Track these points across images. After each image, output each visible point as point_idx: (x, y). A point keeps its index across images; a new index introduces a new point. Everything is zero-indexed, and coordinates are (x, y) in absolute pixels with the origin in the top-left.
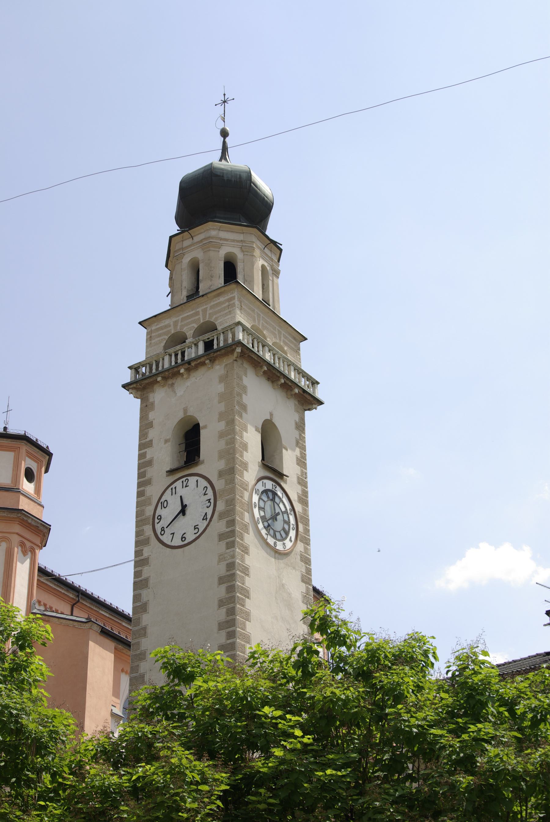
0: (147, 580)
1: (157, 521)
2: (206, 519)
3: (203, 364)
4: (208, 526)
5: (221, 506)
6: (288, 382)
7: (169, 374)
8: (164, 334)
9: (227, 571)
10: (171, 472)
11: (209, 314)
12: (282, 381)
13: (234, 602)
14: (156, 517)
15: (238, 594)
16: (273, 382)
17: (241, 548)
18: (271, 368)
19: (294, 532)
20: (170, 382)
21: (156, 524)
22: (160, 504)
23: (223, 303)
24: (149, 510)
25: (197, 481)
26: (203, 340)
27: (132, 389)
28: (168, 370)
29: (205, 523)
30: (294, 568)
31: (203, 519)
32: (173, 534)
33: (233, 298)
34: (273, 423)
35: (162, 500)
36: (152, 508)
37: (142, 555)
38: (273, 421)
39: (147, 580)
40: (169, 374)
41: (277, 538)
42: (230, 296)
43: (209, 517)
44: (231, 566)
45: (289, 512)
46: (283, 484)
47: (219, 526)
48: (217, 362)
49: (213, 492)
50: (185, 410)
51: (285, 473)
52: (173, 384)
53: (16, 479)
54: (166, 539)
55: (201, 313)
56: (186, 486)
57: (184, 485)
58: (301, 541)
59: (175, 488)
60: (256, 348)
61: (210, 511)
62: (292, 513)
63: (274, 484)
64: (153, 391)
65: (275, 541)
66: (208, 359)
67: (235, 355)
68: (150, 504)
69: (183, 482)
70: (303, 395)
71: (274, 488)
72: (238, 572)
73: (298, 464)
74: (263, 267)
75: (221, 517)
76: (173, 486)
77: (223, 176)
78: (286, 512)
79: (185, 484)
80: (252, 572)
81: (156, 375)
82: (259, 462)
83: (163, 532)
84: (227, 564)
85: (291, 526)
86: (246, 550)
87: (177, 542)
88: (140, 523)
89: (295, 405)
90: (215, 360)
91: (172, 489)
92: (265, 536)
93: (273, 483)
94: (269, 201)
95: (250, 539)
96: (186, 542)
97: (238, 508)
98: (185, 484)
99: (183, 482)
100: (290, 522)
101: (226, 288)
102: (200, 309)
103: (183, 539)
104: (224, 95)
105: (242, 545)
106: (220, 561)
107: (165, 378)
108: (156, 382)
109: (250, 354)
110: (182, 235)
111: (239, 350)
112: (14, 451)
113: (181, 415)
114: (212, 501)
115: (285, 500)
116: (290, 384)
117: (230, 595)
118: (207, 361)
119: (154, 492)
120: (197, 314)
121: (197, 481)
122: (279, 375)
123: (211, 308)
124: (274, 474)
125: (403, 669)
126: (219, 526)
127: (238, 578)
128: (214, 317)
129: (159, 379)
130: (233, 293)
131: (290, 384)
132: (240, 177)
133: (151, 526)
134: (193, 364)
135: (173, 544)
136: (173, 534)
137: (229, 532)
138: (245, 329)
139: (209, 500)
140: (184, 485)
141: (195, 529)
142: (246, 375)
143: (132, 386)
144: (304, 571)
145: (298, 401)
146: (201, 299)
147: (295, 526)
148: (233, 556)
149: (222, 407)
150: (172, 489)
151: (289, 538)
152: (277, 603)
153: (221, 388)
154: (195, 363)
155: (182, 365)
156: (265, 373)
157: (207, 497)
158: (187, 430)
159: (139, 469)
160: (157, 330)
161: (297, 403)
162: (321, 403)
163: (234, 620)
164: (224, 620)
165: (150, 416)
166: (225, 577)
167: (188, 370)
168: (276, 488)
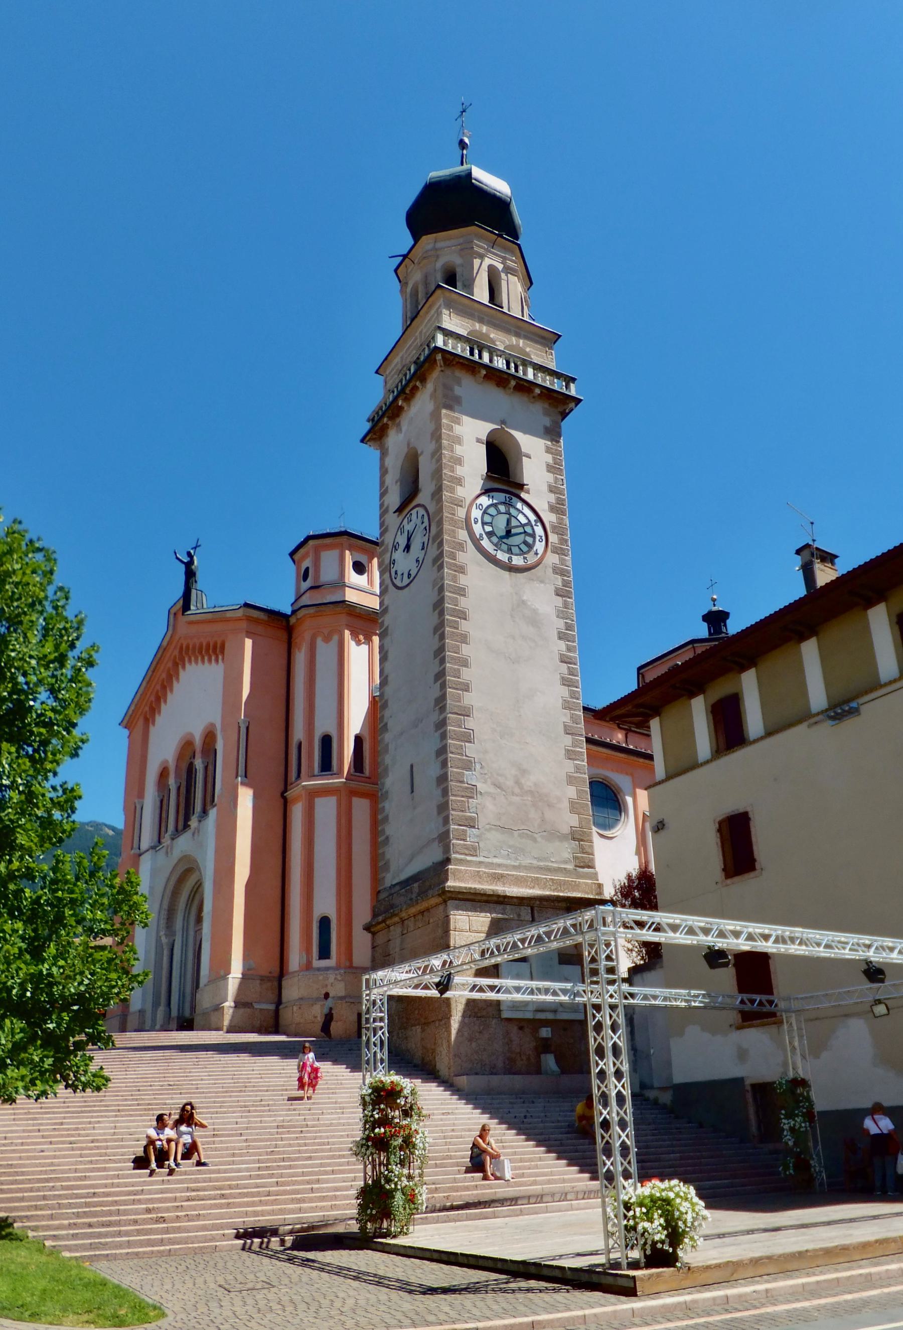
15: (447, 617)
16: (504, 387)
17: (453, 568)
18: (448, 356)
27: (368, 441)
28: (386, 410)
30: (542, 582)
45: (533, 523)
47: (433, 551)
58: (553, 552)
60: (521, 372)
61: (426, 539)
63: (508, 496)
65: (509, 555)
71: (508, 499)
73: (548, 471)
78: (529, 523)
82: (482, 475)
87: (406, 581)
92: (494, 553)
93: (844, 566)
94: (503, 196)
95: (469, 556)
100: (535, 534)
102: (417, 334)
114: (428, 528)
115: (526, 510)
118: (418, 384)
120: (416, 339)
122: (506, 376)
124: (500, 483)
129: (385, 420)
134: (407, 391)
142: (459, 384)
143: (368, 438)
147: (544, 538)
152: (514, 621)
156: (486, 377)
161: (546, 406)
162: (578, 401)
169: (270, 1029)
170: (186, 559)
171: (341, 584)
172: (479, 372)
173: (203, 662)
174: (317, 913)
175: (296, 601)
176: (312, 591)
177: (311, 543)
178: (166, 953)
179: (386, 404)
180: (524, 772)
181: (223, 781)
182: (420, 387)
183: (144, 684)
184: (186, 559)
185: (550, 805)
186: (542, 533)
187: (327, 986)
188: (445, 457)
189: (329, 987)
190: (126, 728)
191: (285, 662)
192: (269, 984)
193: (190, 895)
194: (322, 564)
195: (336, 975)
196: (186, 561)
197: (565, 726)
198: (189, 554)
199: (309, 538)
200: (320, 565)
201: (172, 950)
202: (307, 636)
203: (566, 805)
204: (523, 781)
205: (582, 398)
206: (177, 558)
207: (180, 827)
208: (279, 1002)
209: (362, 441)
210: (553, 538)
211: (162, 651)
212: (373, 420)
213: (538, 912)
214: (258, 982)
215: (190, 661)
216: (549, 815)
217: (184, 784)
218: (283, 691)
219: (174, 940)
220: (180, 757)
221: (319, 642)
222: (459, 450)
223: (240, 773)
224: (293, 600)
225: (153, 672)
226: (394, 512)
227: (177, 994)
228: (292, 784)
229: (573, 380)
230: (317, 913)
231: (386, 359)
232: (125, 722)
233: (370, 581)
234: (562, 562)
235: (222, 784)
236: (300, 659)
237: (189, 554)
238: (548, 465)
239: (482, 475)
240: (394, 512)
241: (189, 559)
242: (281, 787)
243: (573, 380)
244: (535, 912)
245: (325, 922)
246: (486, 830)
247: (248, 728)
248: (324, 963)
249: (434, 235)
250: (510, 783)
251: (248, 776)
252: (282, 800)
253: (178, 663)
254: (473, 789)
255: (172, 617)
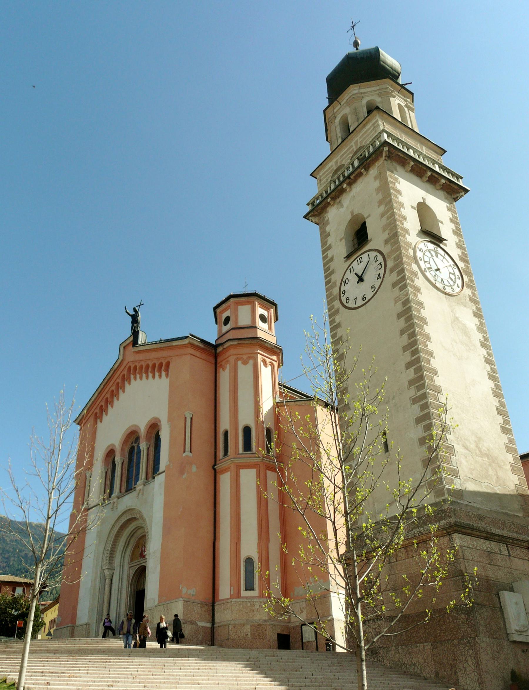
0: (341, 338)
1: (342, 295)
2: (380, 278)
3: (360, 174)
4: (382, 282)
5: (390, 264)
6: (434, 174)
7: (336, 193)
8: (330, 173)
9: (403, 307)
10: (348, 257)
11: (360, 142)
12: (429, 173)
13: (413, 327)
14: (341, 292)
15: (416, 321)
18: (393, 150)
19: (461, 280)
20: (338, 200)
21: (342, 297)
22: (343, 283)
23: (369, 129)
24: (335, 291)
25: (369, 255)
26: (357, 158)
29: (380, 281)
31: (378, 279)
32: (356, 298)
33: (377, 121)
34: (427, 206)
35: (344, 280)
36: (337, 288)
37: (335, 322)
38: (427, 203)
39: (341, 338)
40: (336, 193)
41: (445, 283)
42: (373, 121)
43: (382, 276)
44: (407, 302)
46: (441, 245)
47: (391, 278)
48: (371, 169)
49: (383, 257)
50: (352, 213)
51: (443, 236)
52: (340, 202)
53: (254, 320)
54: (351, 305)
55: (354, 145)
56: (361, 263)
57: (359, 263)
59: (353, 267)
61: (382, 272)
62: (455, 267)
64: (327, 212)
66: (363, 168)
67: (384, 154)
68: (336, 286)
69: (358, 261)
70: (450, 185)
72: (413, 305)
74: (399, 104)
75: (391, 271)
76: (351, 267)
77: (357, 57)
79: (359, 261)
80: (426, 305)
81: (326, 198)
83: (348, 301)
84: (402, 302)
85: (457, 277)
86: (418, 290)
87: (360, 302)
88: (330, 301)
89: (445, 195)
90: (369, 168)
91: (350, 269)
96: (366, 301)
97: (405, 259)
98: (359, 261)
99: (358, 261)
101: (369, 117)
102: (353, 143)
103: (364, 299)
104: (352, 22)
105: (431, 369)
106: (396, 302)
107: (334, 199)
108: (329, 204)
109: (397, 152)
110: (332, 106)
111: (386, 149)
112: (250, 304)
113: (349, 217)
114: (383, 264)
116: (436, 176)
117: (409, 323)
119: (336, 278)
121: (369, 255)
123: (361, 137)
124: (434, 239)
125: (417, 647)
126: (391, 278)
127: (413, 309)
128: (364, 142)
129: (329, 200)
130: (375, 118)
131: (436, 176)
132: (370, 53)
133: (339, 300)
134: (352, 177)
135: (357, 306)
136: (356, 298)
137: (400, 279)
138: (387, 132)
139: (380, 264)
140: (359, 263)
141: (372, 288)
144: (475, 309)
145: (447, 192)
146: (352, 134)
147: (460, 277)
148: (407, 294)
149: (380, 196)
150: (350, 269)
151: (456, 285)
153: (377, 184)
154: (354, 175)
155: (344, 181)
157: (378, 263)
158: (356, 230)
159: (324, 266)
160: (323, 174)
162: (466, 191)
163: (416, 340)
164: (407, 344)
165: (327, 229)
166: (402, 312)
167: (350, 184)
168: (437, 248)
169: (208, 643)
170: (132, 313)
171: (254, 327)
172: (409, 163)
173: (147, 378)
174: (244, 555)
175: (218, 339)
176: (233, 330)
177: (232, 300)
178: (108, 582)
179: (326, 192)
180: (480, 439)
181: (170, 455)
182: (364, 174)
183: (96, 394)
184: (132, 313)
185: (500, 467)
186: (459, 274)
187: (253, 611)
188: (396, 214)
189: (255, 612)
190: (78, 424)
191: (214, 377)
192: (206, 607)
193: (126, 541)
194: (239, 314)
195: (261, 603)
196: (131, 314)
197: (497, 409)
198: (135, 310)
199: (231, 297)
200: (238, 314)
201: (111, 580)
202: (232, 359)
203: (509, 467)
204: (480, 446)
205: (469, 189)
206: (126, 312)
207: (123, 490)
208: (213, 622)
209: (305, 217)
210: (466, 278)
211: (113, 372)
212: (313, 204)
213: (512, 550)
214: (199, 605)
215: (135, 379)
216: (500, 474)
217: (126, 461)
218: (213, 398)
219: (113, 573)
220: (125, 442)
221: (240, 363)
222: (404, 212)
223: (186, 450)
224: (217, 338)
225: (104, 386)
226: (344, 258)
227: (115, 613)
228: (220, 460)
229: (462, 178)
230: (244, 555)
231: (321, 164)
232: (77, 422)
233: (270, 328)
234: (474, 294)
235: (170, 460)
236: (225, 376)
237: (135, 310)
238: (453, 230)
239: (418, 230)
240: (344, 258)
241: (134, 313)
242: (213, 463)
243: (462, 178)
244: (509, 548)
245: (249, 561)
246: (465, 480)
247: (191, 419)
248: (250, 593)
249: (360, 84)
250: (472, 446)
251: (192, 451)
252: (213, 471)
253: (125, 379)
254: (452, 448)
255: (122, 348)
